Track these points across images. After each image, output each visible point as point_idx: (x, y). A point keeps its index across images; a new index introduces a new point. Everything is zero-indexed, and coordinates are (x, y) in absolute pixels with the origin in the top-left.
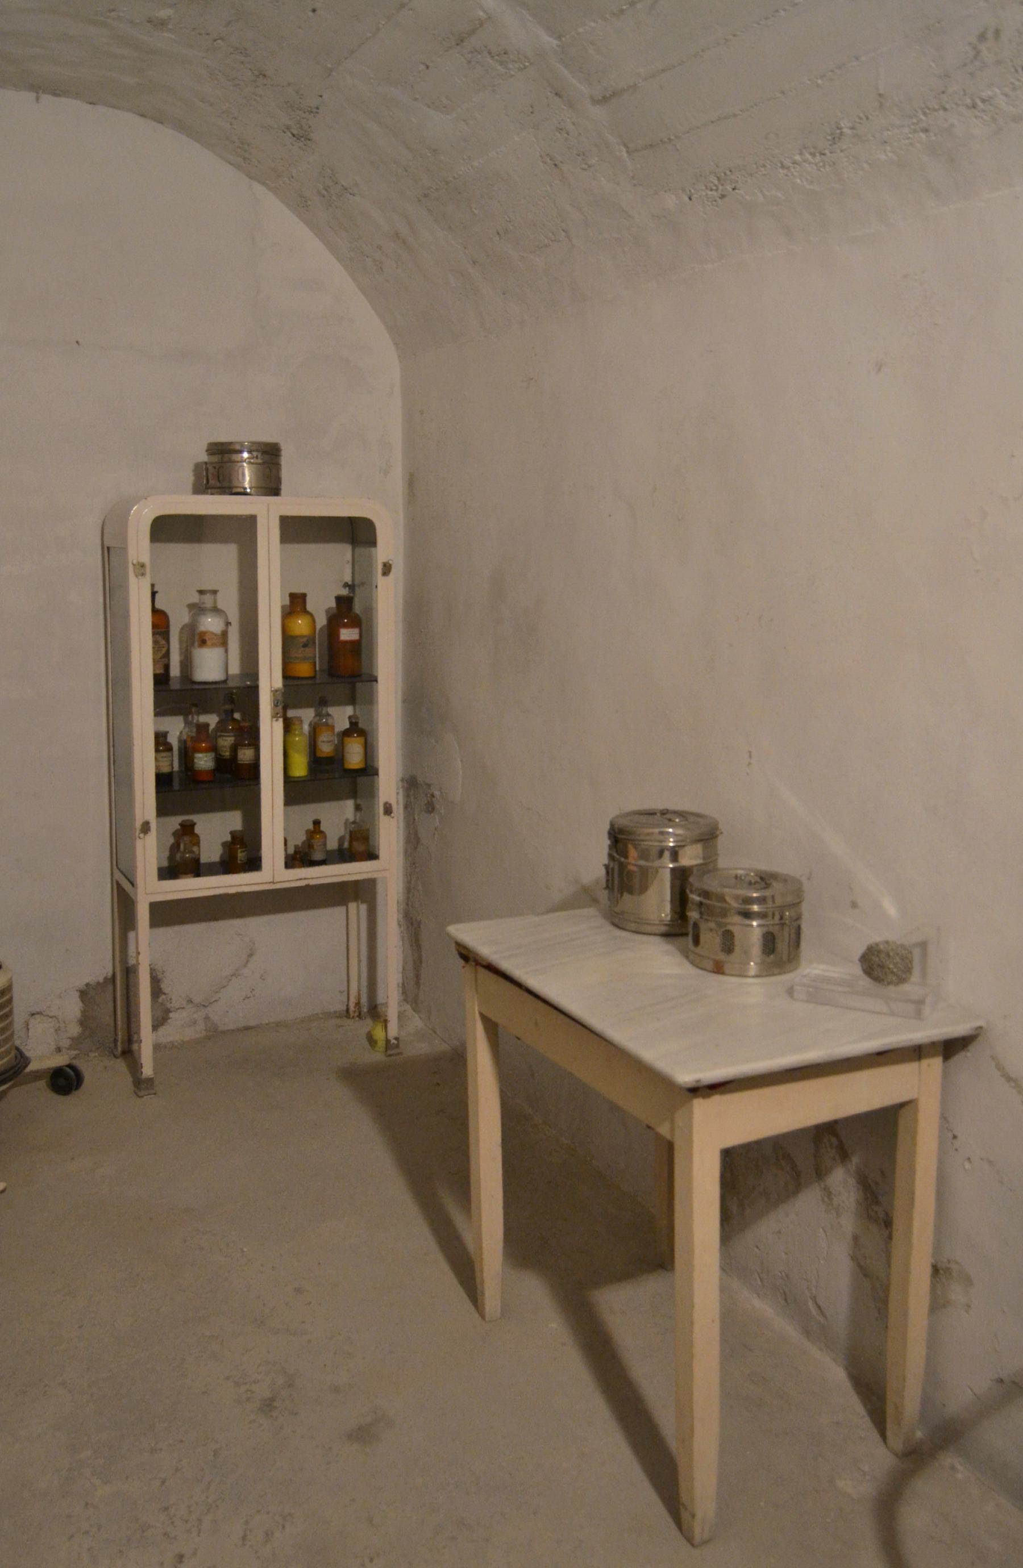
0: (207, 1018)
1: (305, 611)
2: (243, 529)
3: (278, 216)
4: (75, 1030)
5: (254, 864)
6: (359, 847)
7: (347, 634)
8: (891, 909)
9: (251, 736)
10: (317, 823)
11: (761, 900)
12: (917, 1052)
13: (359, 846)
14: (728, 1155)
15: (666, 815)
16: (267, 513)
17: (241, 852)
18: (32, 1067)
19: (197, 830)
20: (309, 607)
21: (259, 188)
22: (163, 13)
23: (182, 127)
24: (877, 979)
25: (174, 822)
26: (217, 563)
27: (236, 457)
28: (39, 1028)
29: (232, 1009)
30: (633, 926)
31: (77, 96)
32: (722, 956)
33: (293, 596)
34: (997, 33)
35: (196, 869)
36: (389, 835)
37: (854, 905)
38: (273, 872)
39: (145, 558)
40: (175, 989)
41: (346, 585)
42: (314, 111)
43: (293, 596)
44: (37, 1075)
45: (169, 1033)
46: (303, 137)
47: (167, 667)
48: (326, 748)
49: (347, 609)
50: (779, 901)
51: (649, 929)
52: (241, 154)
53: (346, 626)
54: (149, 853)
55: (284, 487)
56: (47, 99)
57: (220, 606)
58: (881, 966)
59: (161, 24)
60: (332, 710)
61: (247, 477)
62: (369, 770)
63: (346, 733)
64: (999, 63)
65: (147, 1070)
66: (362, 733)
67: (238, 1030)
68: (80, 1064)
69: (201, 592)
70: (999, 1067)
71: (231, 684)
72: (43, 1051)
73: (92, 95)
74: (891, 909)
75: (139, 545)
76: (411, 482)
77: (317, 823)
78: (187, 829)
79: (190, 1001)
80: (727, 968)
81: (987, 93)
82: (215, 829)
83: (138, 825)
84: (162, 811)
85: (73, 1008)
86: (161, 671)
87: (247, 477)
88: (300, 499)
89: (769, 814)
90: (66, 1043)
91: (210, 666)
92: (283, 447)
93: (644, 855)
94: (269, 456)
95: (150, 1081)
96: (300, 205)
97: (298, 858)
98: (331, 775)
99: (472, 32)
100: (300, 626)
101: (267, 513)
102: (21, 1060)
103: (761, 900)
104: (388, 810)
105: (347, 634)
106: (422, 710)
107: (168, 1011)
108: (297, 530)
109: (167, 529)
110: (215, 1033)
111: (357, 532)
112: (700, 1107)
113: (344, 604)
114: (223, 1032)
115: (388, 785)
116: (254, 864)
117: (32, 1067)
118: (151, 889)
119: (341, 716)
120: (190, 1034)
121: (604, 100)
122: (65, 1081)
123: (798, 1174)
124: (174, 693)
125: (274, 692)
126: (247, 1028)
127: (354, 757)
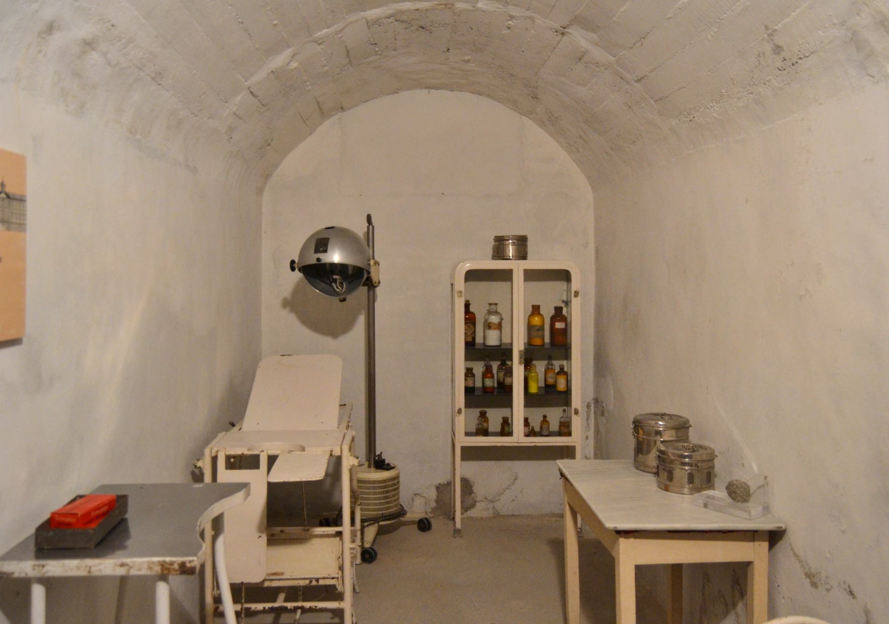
0: (494, 507)
1: (539, 314)
2: (506, 276)
3: (534, 130)
4: (433, 504)
5: (510, 434)
6: (564, 430)
7: (559, 325)
8: (756, 468)
9: (509, 372)
10: (545, 417)
11: (689, 457)
12: (751, 535)
13: (565, 429)
14: (639, 569)
15: (662, 416)
16: (518, 268)
17: (506, 429)
18: (409, 516)
19: (487, 415)
20: (542, 312)
21: (524, 118)
22: (467, 58)
23: (488, 96)
24: (734, 499)
25: (476, 412)
26: (496, 289)
27: (507, 242)
28: (418, 502)
29: (505, 505)
30: (642, 468)
31: (445, 88)
32: (668, 483)
33: (533, 307)
34: (763, 54)
35: (485, 432)
36: (577, 424)
37: (743, 465)
38: (518, 437)
39: (462, 289)
40: (479, 490)
41: (563, 301)
42: (537, 88)
43: (533, 307)
44: (412, 523)
45: (472, 513)
46: (535, 97)
47: (474, 339)
48: (551, 381)
49: (558, 314)
50: (699, 458)
51: (650, 470)
52: (513, 105)
53: (559, 321)
54: (461, 423)
55: (529, 255)
56: (433, 91)
57: (499, 311)
58: (735, 492)
59: (468, 61)
60: (554, 362)
61: (511, 251)
62: (567, 393)
63: (558, 373)
64: (768, 66)
65: (458, 525)
66: (566, 374)
67: (508, 516)
68: (432, 521)
69: (490, 304)
70: (793, 550)
71: (503, 347)
72: (416, 511)
73: (450, 87)
74: (756, 468)
75: (460, 284)
76: (597, 251)
77: (545, 417)
78: (483, 415)
79: (486, 498)
80: (670, 488)
81: (768, 79)
82: (495, 417)
83: (457, 410)
84: (468, 405)
85: (433, 494)
86: (470, 339)
87: (511, 251)
88: (533, 263)
89: (721, 422)
90: (429, 510)
91: (493, 338)
92: (529, 237)
93: (649, 435)
94: (522, 242)
95: (459, 531)
96: (542, 124)
97: (531, 433)
98: (552, 395)
99: (583, 56)
100: (536, 320)
101: (518, 268)
102: (402, 513)
103: (689, 457)
104: (576, 412)
105: (559, 325)
106: (601, 365)
107: (476, 502)
108: (531, 275)
109: (472, 276)
110: (497, 515)
111: (565, 276)
112: (623, 543)
113: (558, 310)
114: (503, 516)
115: (577, 400)
116: (510, 434)
117: (409, 516)
118: (463, 441)
119: (557, 364)
120: (485, 514)
121: (638, 81)
122: (424, 525)
123: (726, 605)
124: (473, 349)
125: (520, 352)
126: (513, 515)
127: (561, 385)
